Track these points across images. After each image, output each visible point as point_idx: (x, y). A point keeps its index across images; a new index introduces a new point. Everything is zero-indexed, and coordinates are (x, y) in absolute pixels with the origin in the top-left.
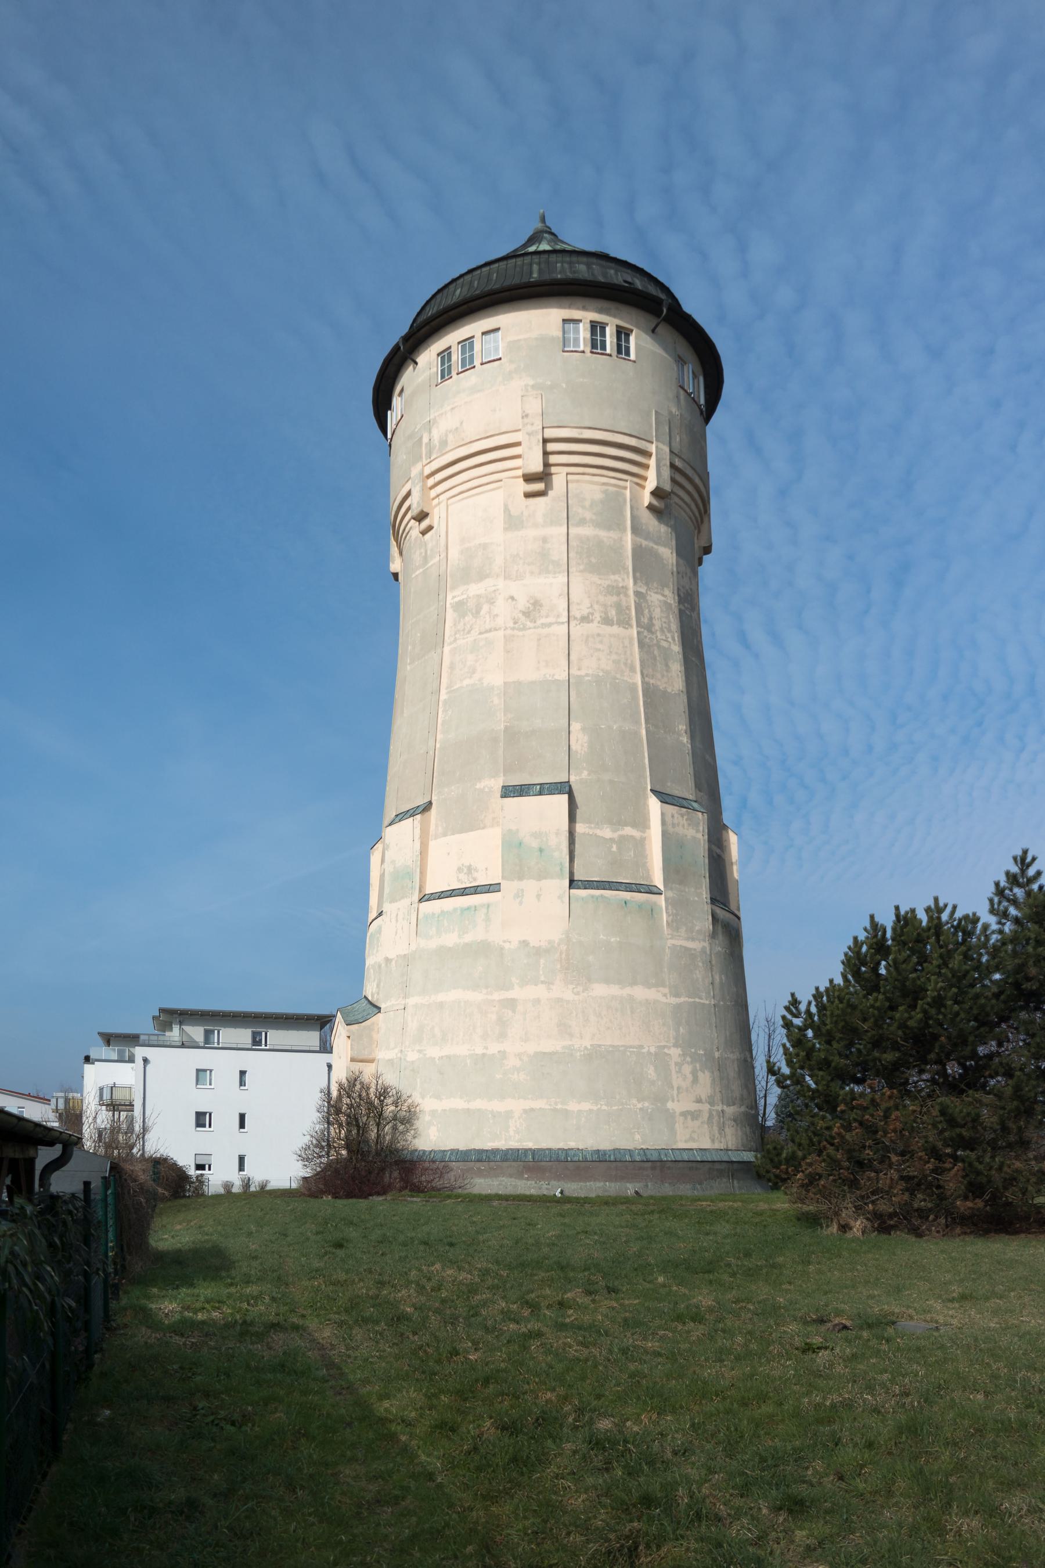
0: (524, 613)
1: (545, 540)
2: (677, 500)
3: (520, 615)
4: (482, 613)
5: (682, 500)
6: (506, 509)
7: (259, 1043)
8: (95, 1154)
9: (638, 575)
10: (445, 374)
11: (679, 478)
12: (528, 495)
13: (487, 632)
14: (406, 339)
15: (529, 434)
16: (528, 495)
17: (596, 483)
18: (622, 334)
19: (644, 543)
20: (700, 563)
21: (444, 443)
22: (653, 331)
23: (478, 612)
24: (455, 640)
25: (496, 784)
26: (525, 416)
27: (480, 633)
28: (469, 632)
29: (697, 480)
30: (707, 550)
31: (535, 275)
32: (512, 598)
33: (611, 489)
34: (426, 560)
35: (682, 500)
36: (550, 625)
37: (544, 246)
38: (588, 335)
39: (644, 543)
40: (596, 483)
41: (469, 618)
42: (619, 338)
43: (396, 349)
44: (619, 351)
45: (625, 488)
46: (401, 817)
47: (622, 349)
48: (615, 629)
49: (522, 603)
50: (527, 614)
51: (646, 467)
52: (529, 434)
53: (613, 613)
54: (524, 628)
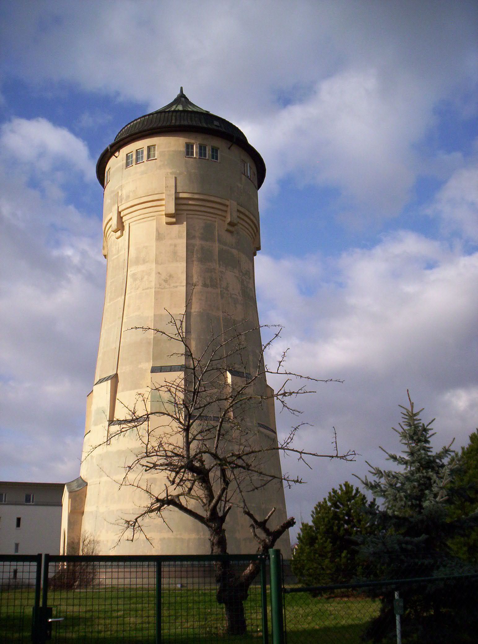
0: (164, 281)
1: (175, 246)
2: (241, 226)
3: (163, 282)
4: (145, 279)
5: (243, 226)
6: (157, 230)
7: (29, 501)
8: (226, 574)
9: (221, 263)
10: (127, 165)
11: (241, 216)
12: (168, 223)
13: (146, 289)
14: (112, 146)
15: (168, 195)
16: (168, 223)
17: (201, 219)
18: (215, 150)
19: (225, 248)
20: (255, 255)
21: (128, 197)
22: (229, 148)
23: (142, 279)
24: (131, 292)
25: (149, 366)
26: (167, 187)
27: (143, 290)
28: (137, 289)
29: (252, 217)
30: (259, 248)
31: (173, 121)
32: (159, 273)
33: (208, 222)
34: (118, 252)
35: (243, 226)
36: (176, 287)
37: (180, 108)
38: (198, 150)
39: (225, 248)
40: (201, 219)
41: (138, 282)
42: (212, 152)
43: (107, 151)
44: (213, 158)
45: (215, 221)
46: (101, 381)
47: (214, 155)
48: (210, 289)
49: (164, 276)
50: (166, 281)
51: (226, 211)
52: (168, 195)
53: (208, 282)
54: (164, 288)
